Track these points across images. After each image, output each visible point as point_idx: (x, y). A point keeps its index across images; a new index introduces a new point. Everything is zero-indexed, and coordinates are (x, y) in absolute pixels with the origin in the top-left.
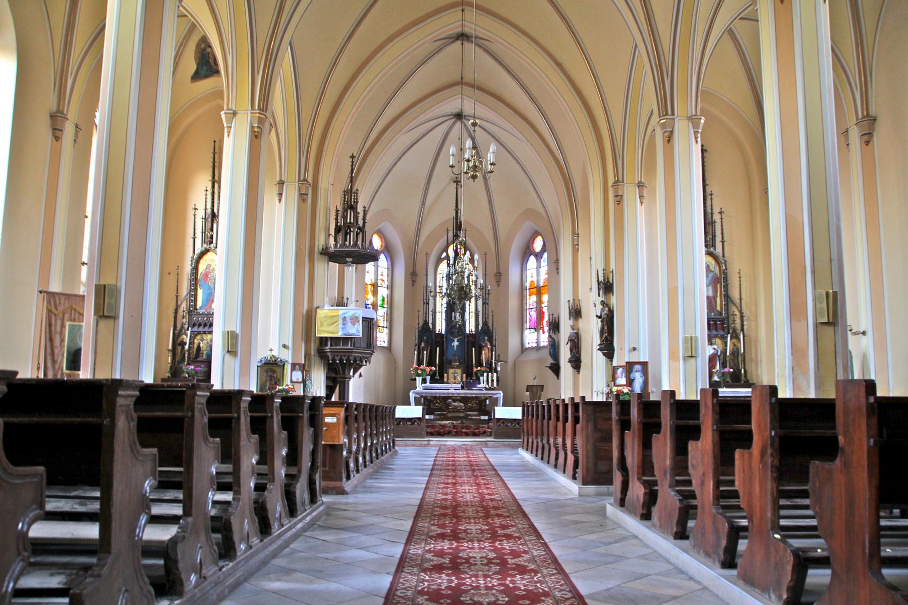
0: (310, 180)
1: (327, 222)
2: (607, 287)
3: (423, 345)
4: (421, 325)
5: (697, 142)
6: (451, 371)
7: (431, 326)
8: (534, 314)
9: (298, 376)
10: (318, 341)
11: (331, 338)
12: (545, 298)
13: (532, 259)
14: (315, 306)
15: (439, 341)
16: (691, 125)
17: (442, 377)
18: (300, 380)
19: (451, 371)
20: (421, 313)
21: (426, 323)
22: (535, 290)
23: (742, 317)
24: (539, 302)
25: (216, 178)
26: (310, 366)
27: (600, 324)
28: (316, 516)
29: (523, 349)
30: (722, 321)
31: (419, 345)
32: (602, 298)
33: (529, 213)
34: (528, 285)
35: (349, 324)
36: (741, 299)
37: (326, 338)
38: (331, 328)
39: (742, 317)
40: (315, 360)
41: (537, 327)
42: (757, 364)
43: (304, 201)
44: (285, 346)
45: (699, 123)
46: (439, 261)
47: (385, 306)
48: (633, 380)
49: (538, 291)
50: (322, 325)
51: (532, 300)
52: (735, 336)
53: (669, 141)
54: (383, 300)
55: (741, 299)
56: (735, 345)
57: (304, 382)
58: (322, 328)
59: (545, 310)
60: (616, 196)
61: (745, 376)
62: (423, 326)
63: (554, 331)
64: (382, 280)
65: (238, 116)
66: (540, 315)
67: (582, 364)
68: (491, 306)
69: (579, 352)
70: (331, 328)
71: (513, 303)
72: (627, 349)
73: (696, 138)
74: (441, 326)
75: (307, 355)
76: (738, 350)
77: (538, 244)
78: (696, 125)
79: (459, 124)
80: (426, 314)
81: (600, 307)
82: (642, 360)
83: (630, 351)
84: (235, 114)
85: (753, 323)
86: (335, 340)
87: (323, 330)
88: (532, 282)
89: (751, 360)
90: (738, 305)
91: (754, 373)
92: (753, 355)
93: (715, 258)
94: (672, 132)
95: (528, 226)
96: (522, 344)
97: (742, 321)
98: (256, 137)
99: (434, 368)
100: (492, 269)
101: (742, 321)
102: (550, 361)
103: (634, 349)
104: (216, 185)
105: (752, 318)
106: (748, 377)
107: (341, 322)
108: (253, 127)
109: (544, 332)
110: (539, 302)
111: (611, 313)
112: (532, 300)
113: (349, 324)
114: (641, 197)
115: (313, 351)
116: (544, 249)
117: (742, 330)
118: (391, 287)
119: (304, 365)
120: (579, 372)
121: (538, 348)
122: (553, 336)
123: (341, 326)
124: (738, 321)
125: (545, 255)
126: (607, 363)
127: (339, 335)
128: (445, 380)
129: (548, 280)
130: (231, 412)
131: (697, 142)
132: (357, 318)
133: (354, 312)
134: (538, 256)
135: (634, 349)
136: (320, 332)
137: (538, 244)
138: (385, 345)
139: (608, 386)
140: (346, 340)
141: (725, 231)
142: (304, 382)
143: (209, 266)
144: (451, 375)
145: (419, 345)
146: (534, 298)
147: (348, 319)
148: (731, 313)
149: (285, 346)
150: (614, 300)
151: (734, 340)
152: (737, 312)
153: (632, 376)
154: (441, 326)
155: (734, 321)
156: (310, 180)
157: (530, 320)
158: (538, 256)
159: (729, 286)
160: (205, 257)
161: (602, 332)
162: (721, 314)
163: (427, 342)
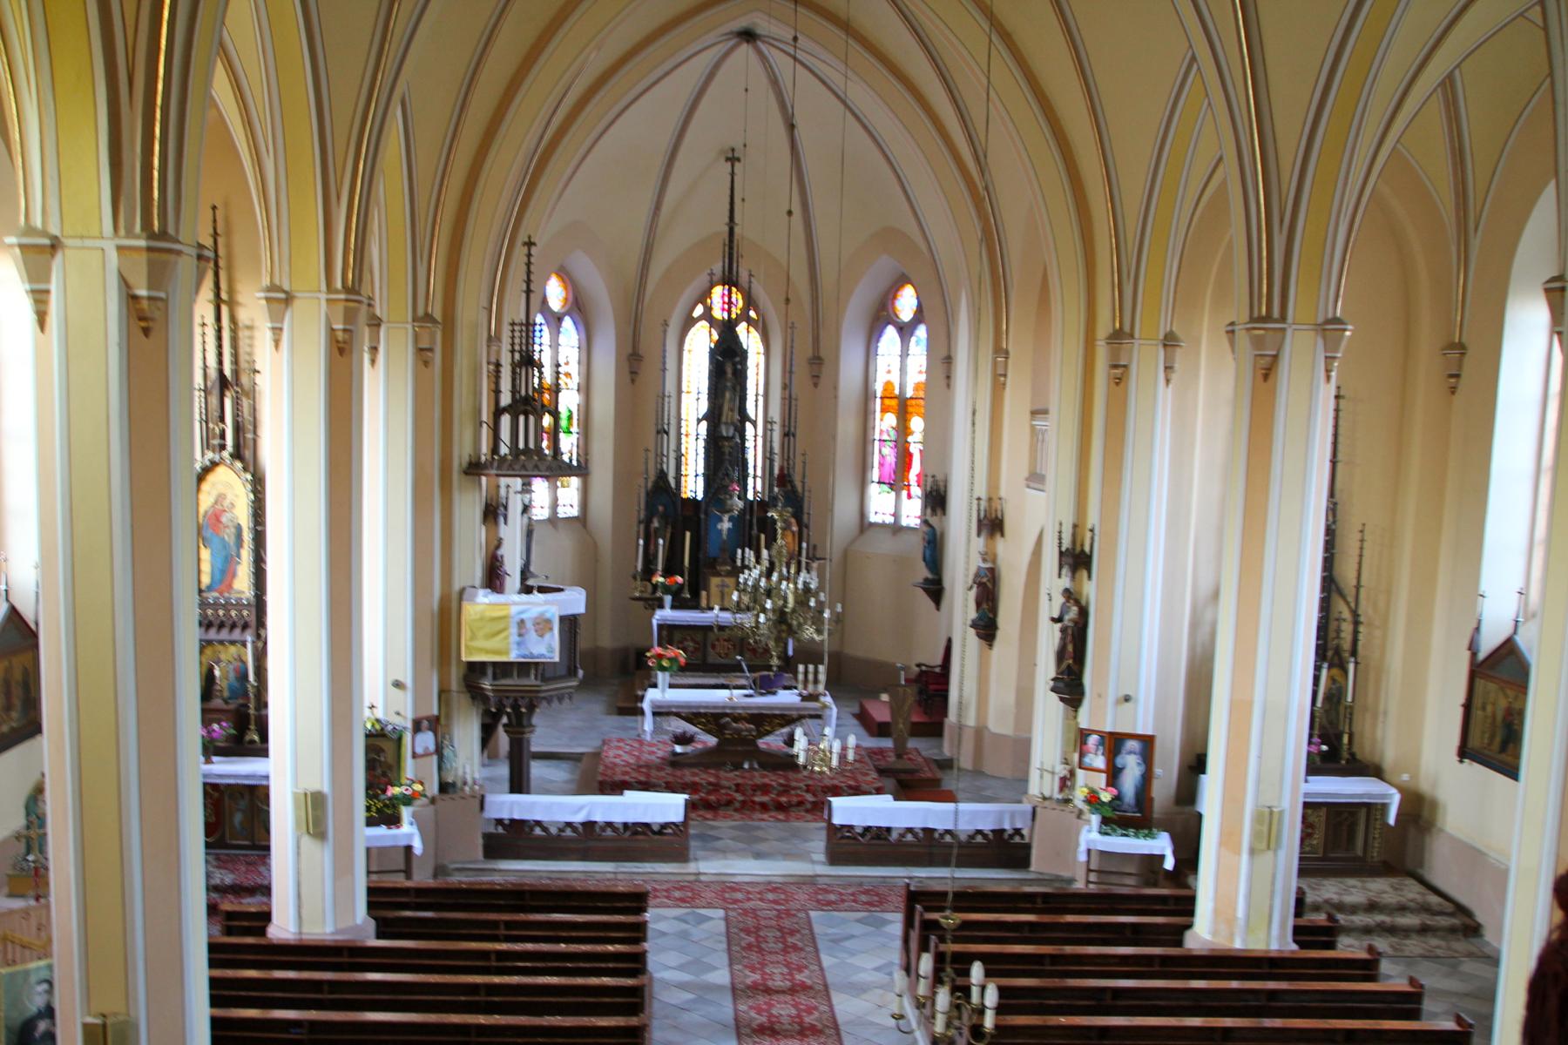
0: (438, 315)
1: (475, 395)
2: (1077, 560)
3: (656, 524)
4: (652, 478)
5: (1328, 378)
6: (715, 581)
7: (673, 484)
8: (889, 452)
9: (427, 740)
10: (463, 670)
11: (495, 664)
12: (917, 424)
13: (891, 333)
14: (457, 587)
15: (690, 516)
16: (1320, 342)
17: (696, 594)
18: (432, 747)
19: (715, 581)
20: (652, 455)
21: (662, 475)
22: (894, 403)
23: (1356, 623)
24: (903, 429)
25: (224, 296)
26: (449, 717)
27: (1058, 635)
29: (864, 526)
31: (648, 522)
32: (1065, 582)
33: (888, 238)
34: (879, 388)
35: (532, 635)
37: (483, 664)
38: (494, 643)
39: (1356, 623)
40: (461, 701)
41: (896, 482)
42: (1375, 716)
43: (426, 363)
44: (398, 685)
45: (1342, 336)
46: (689, 322)
47: (575, 429)
48: (1121, 770)
49: (903, 409)
50: (473, 637)
51: (885, 423)
53: (1266, 377)
54: (570, 418)
55: (1358, 587)
57: (439, 750)
58: (476, 644)
59: (915, 449)
60: (1115, 366)
62: (656, 484)
63: (934, 512)
64: (568, 375)
65: (297, 304)
66: (905, 459)
67: (1000, 634)
68: (800, 443)
69: (994, 610)
70: (494, 643)
71: (847, 427)
72: (1111, 699)
73: (1328, 371)
74: (693, 486)
75: (443, 692)
77: (906, 303)
78: (1331, 344)
79: (745, 49)
80: (660, 455)
81: (1059, 600)
82: (1140, 732)
83: (1117, 702)
84: (289, 299)
85: (1378, 633)
86: (503, 669)
87: (477, 648)
88: (888, 385)
90: (1351, 599)
94: (1275, 357)
95: (884, 266)
96: (862, 514)
97: (1356, 633)
98: (341, 351)
99: (679, 579)
100: (804, 350)
102: (924, 573)
103: (1127, 699)
104: (225, 310)
106: (1355, 749)
107: (514, 630)
108: (331, 331)
109: (909, 496)
110: (903, 429)
111: (1084, 612)
112: (885, 423)
113: (532, 635)
115: (455, 683)
116: (919, 317)
117: (1354, 653)
118: (586, 389)
119: (437, 719)
120: (991, 646)
121: (896, 529)
122: (933, 521)
123: (514, 638)
124: (1347, 628)
125: (921, 331)
126: (1066, 718)
127: (513, 657)
128: (704, 603)
129: (927, 386)
131: (1328, 378)
132: (549, 621)
133: (540, 609)
134: (905, 331)
135: (1127, 699)
136: (470, 650)
137: (906, 303)
138: (574, 512)
139: (1066, 762)
140: (523, 668)
141: (1341, 439)
142: (439, 750)
143: (220, 498)
144: (714, 590)
145: (648, 522)
146: (891, 420)
147: (529, 625)
148: (1334, 615)
149: (398, 685)
150: (1090, 590)
151: (1335, 671)
152: (1346, 614)
153: (1119, 761)
154: (693, 486)
156: (438, 315)
157: (881, 465)
158: (905, 331)
159: (1337, 557)
160: (211, 478)
161: (1061, 655)
163: (665, 518)
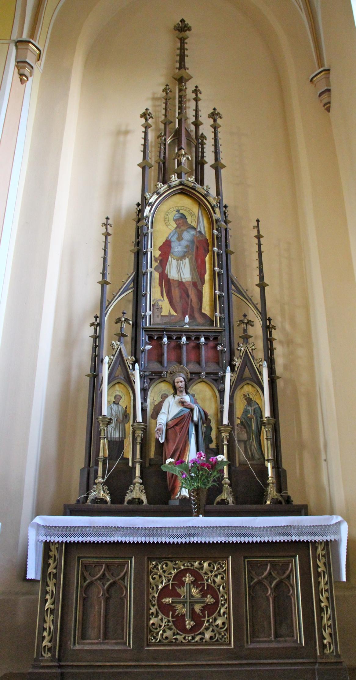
28: (40, 673)
30: (214, 338)
36: (262, 286)
52: (247, 376)
55: (262, 286)
56: (249, 401)
61: (281, 485)
76: (259, 412)
85: (301, 352)
89: (301, 446)
91: (309, 479)
92: (306, 434)
93: (200, 200)
101: (269, 341)
105: (298, 340)
114: (21, 63)
130: (336, 544)
155: (246, 338)
162: (212, 322)
